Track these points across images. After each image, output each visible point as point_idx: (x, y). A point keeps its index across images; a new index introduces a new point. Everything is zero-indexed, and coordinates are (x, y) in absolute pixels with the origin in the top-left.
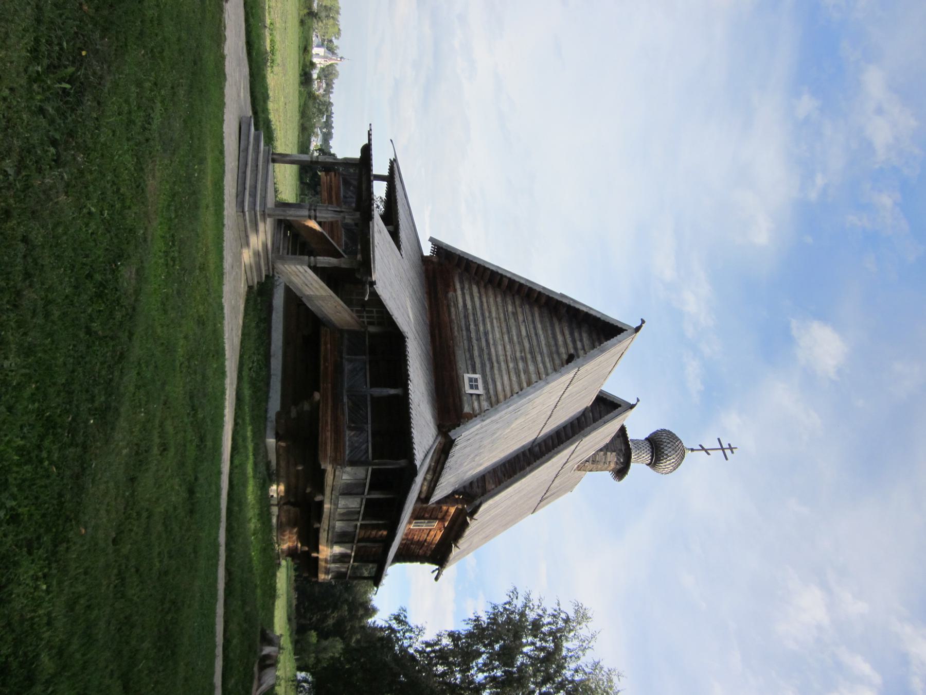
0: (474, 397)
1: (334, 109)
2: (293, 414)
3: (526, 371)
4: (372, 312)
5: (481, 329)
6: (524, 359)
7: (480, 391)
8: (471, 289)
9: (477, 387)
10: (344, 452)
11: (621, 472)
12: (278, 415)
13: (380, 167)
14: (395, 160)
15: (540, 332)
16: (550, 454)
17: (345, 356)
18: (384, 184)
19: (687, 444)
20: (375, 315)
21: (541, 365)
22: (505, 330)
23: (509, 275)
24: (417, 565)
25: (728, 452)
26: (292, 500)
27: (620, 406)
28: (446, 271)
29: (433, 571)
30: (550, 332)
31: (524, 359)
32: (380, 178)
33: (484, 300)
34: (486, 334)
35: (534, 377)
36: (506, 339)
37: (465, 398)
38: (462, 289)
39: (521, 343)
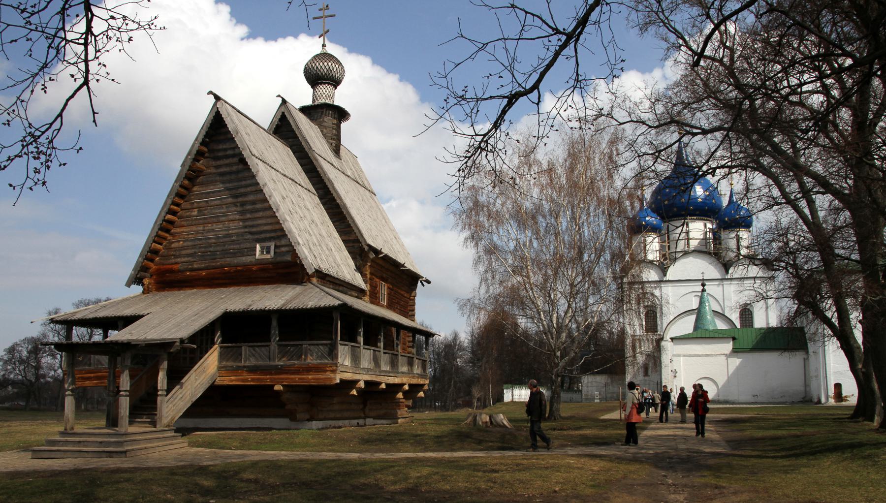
0: (277, 250)
3: (253, 203)
11: (341, 114)
16: (326, 181)
17: (243, 364)
19: (318, 50)
21: (249, 189)
25: (327, 13)
26: (361, 406)
27: (283, 113)
28: (159, 272)
29: (423, 285)
35: (259, 196)
37: (279, 259)
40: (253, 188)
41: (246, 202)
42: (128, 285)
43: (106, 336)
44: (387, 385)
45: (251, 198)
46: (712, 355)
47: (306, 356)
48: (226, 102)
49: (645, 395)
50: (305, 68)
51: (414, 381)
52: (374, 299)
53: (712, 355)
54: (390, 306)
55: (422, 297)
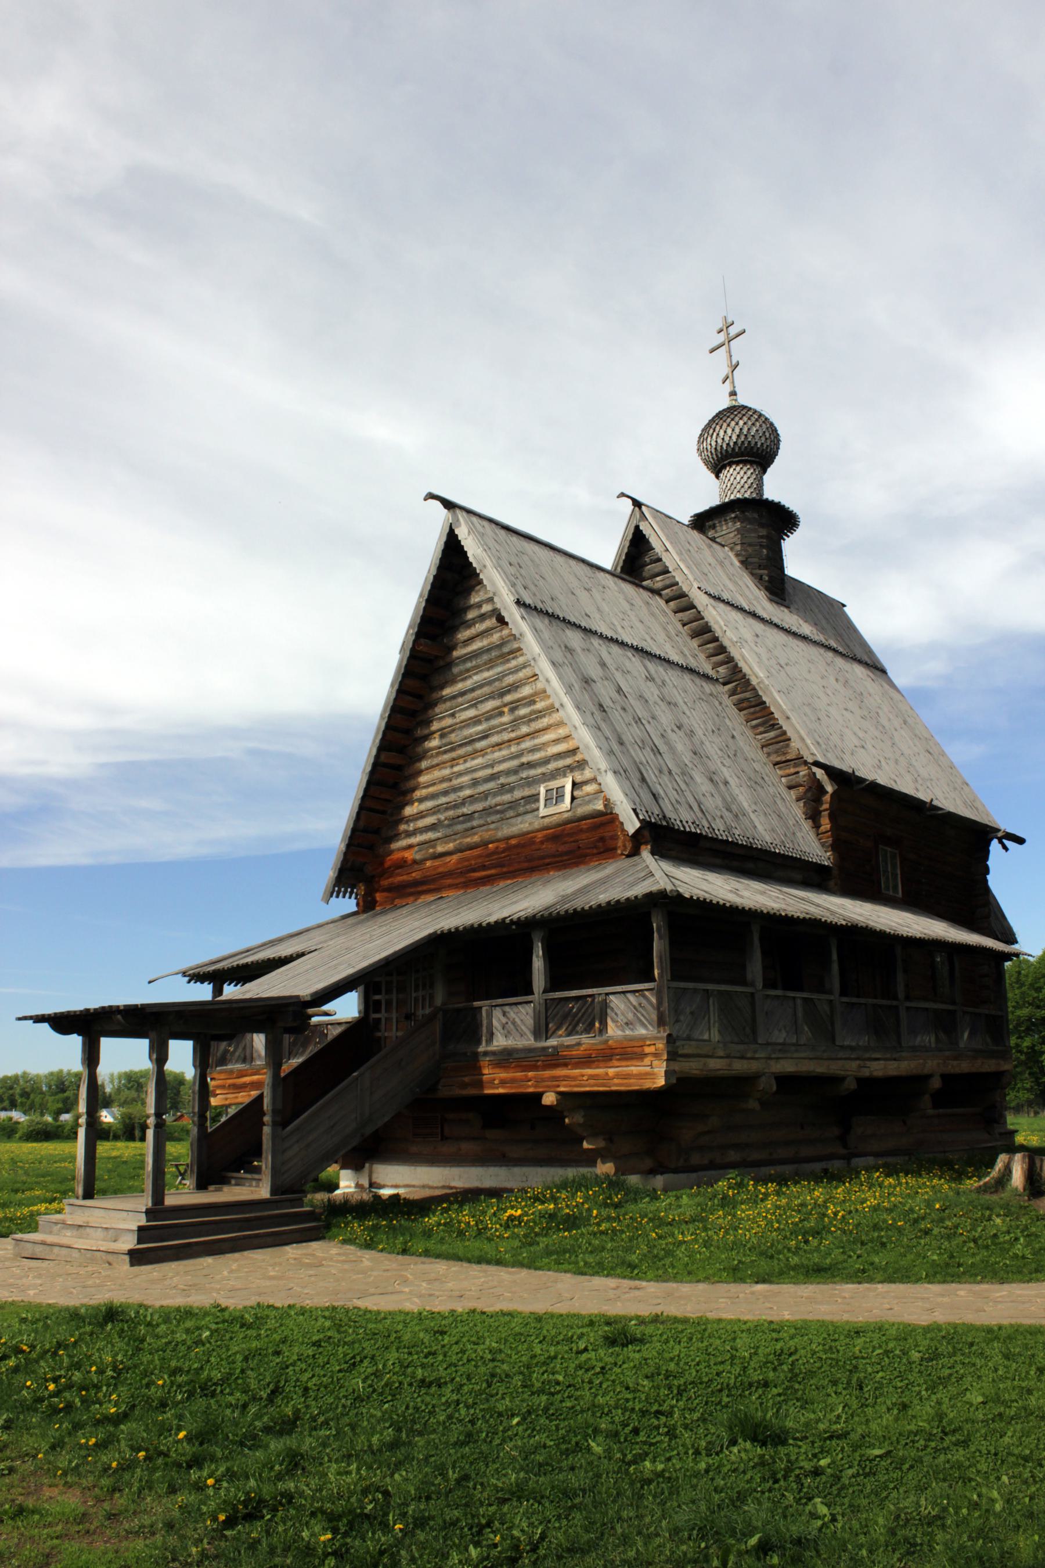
4: (416, 999)
5: (468, 792)
6: (514, 706)
8: (408, 820)
15: (468, 684)
19: (725, 403)
20: (420, 993)
22: (469, 749)
25: (733, 330)
27: (637, 527)
28: (367, 867)
30: (469, 665)
31: (514, 706)
34: (475, 783)
36: (483, 744)
37: (581, 811)
39: (489, 716)
41: (518, 700)
43: (218, 991)
45: (526, 691)
46: (741, 610)
49: (978, 1454)
51: (964, 1066)
53: (741, 610)
55: (1005, 875)
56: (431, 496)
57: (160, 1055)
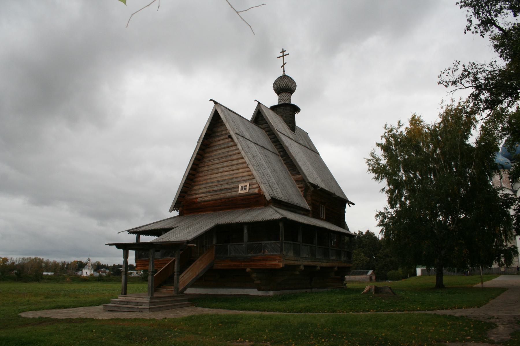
0: (251, 187)
1: (117, 264)
2: (258, 282)
7: (247, 184)
8: (196, 190)
9: (246, 186)
10: (276, 255)
11: (296, 109)
12: (259, 290)
13: (132, 239)
14: (128, 231)
18: (141, 236)
19: (281, 74)
21: (234, 152)
23: (188, 170)
24: (346, 215)
28: (186, 202)
32: (138, 238)
33: (201, 182)
34: (218, 181)
37: (251, 192)
38: (196, 194)
40: (237, 151)
42: (170, 211)
44: (321, 267)
45: (235, 157)
47: (264, 250)
48: (221, 105)
50: (273, 87)
51: (343, 265)
52: (316, 215)
54: (328, 220)
56: (211, 100)
57: (126, 256)
